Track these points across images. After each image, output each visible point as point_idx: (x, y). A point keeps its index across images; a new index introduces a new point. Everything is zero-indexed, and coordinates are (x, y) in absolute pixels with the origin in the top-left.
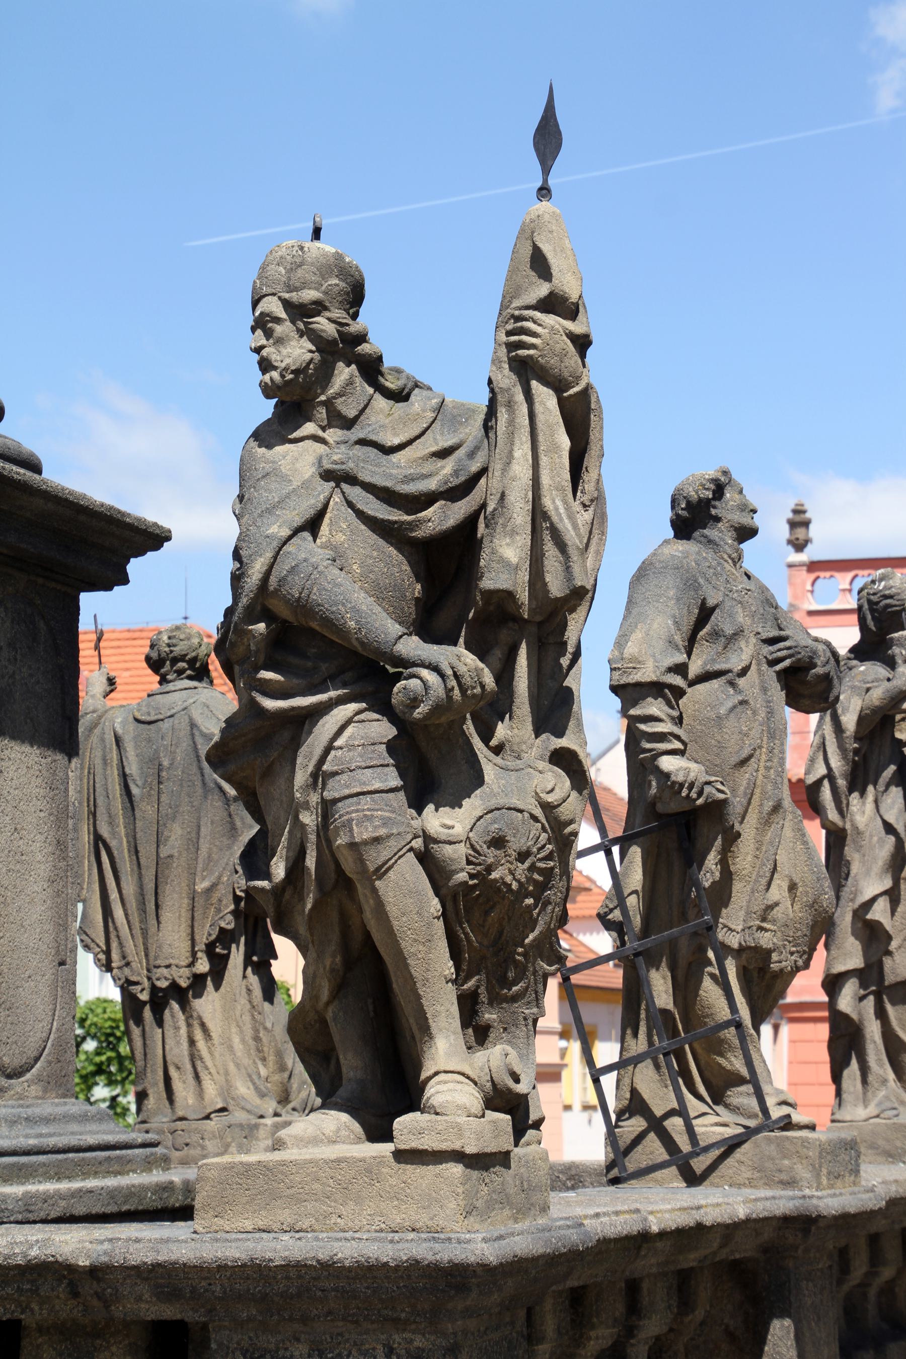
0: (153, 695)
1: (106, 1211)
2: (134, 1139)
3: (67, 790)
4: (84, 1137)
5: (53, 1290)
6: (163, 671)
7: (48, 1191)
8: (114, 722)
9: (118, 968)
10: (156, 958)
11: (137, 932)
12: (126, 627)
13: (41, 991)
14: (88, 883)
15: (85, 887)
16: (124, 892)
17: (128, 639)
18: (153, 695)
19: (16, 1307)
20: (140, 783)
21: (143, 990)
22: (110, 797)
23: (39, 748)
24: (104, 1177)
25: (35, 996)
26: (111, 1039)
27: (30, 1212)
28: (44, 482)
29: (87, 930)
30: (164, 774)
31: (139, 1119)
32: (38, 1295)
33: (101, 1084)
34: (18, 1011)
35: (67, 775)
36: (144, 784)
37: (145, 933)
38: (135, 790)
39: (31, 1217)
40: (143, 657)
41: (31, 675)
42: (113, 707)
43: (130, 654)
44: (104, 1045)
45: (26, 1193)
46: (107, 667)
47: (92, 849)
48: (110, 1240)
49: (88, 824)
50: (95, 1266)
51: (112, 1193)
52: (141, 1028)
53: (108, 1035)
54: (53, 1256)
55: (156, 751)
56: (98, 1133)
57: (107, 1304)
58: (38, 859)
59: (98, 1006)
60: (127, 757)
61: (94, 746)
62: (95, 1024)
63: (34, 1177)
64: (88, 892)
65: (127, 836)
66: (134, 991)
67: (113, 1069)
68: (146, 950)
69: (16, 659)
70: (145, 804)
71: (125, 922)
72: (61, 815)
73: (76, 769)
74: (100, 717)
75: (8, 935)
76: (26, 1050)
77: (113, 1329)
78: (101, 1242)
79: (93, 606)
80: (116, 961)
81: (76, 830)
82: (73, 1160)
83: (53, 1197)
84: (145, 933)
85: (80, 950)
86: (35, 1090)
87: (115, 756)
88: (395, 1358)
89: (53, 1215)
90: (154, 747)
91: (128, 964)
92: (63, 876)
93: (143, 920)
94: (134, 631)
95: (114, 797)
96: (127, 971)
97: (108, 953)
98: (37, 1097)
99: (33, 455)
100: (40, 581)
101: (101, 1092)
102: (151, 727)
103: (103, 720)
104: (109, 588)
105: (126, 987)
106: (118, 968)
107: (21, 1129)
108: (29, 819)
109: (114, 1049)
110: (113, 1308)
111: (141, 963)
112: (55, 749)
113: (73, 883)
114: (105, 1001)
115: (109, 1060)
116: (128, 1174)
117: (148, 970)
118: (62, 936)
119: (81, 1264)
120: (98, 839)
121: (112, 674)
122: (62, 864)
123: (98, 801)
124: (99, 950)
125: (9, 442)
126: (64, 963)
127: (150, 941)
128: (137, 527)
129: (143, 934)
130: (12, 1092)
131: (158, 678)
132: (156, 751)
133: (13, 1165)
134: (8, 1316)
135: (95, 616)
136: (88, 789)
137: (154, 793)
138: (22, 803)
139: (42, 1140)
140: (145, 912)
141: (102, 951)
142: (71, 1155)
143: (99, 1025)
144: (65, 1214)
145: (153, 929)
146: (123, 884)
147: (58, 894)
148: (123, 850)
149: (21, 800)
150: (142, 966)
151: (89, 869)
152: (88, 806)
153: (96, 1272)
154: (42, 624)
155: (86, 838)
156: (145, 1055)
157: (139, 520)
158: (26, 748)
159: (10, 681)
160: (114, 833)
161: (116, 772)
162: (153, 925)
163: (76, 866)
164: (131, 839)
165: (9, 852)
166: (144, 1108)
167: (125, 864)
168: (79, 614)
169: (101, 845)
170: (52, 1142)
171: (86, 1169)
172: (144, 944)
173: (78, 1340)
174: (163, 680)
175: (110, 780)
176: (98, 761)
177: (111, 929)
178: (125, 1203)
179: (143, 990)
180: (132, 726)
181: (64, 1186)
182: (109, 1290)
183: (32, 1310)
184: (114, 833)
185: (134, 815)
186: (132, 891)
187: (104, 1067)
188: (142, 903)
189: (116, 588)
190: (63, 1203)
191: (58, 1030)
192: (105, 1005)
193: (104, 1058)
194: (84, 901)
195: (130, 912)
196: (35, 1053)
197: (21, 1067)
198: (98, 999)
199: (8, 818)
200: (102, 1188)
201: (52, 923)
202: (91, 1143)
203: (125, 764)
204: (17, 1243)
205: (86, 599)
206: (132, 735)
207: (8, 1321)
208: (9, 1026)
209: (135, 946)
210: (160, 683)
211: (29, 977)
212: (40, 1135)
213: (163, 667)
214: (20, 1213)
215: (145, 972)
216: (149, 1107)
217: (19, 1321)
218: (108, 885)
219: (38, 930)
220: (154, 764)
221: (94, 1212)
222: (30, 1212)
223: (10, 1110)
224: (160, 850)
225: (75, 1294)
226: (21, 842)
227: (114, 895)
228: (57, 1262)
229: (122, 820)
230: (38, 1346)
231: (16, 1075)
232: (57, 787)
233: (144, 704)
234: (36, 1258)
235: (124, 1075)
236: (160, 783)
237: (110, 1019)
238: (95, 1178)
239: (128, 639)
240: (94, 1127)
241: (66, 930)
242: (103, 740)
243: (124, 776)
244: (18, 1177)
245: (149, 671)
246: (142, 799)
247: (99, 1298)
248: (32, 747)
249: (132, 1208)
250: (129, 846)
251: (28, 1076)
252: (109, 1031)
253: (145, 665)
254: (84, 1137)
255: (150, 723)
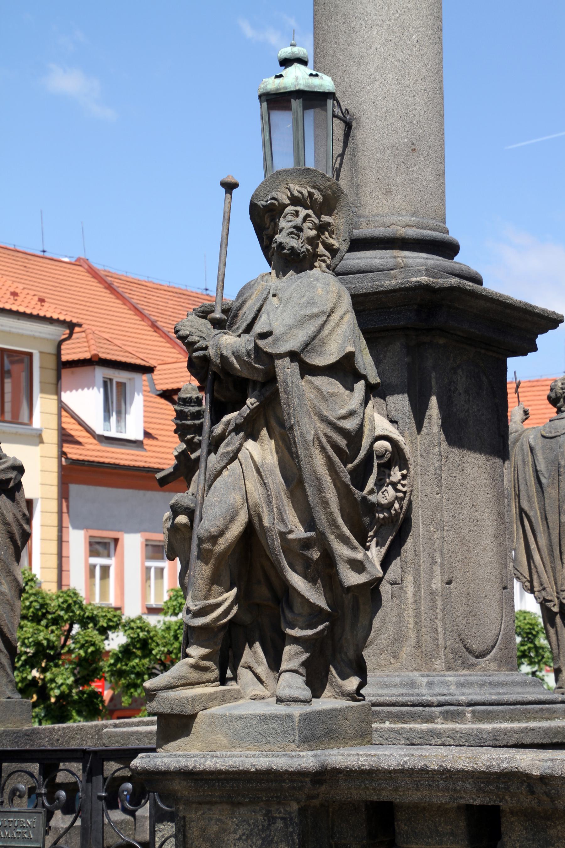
0: (553, 420)
1: (543, 742)
2: (556, 698)
3: (503, 480)
4: (525, 696)
5: (518, 789)
6: (559, 405)
7: (507, 728)
8: (529, 438)
9: (538, 591)
10: (562, 585)
11: (549, 569)
12: (528, 379)
13: (493, 604)
14: (517, 538)
15: (515, 541)
16: (539, 544)
17: (529, 387)
18: (553, 420)
19: (496, 798)
20: (546, 476)
21: (554, 605)
22: (528, 485)
23: (485, 455)
24: (540, 721)
25: (490, 607)
26: (530, 636)
27: (497, 740)
28: (485, 290)
29: (517, 568)
30: (562, 470)
31: (558, 686)
32: (509, 791)
33: (526, 663)
34: (480, 617)
35: (503, 471)
36: (549, 476)
37: (554, 569)
38: (544, 480)
39: (498, 743)
40: (546, 397)
41: (479, 410)
42: (528, 429)
43: (530, 396)
44: (526, 639)
45: (493, 729)
46: (524, 404)
47: (518, 517)
48: (551, 760)
49: (515, 502)
50: (543, 776)
51: (547, 731)
52: (555, 629)
53: (528, 634)
54: (516, 768)
55: (556, 456)
56: (534, 693)
57: (553, 801)
58: (487, 524)
59: (520, 616)
60: (538, 460)
61: (517, 453)
62: (519, 627)
63: (497, 719)
64: (517, 544)
65: (540, 509)
66: (549, 606)
67: (532, 654)
68: (555, 580)
69: (469, 401)
70: (550, 489)
71: (541, 562)
72: (500, 496)
73: (508, 467)
74: (520, 435)
75: (471, 570)
76: (486, 641)
77: (557, 815)
78: (546, 761)
79: (516, 366)
80: (537, 588)
81: (509, 505)
82: (520, 710)
83: (510, 732)
84: (554, 569)
85: (515, 580)
86: (493, 666)
87: (530, 459)
88: (254, 847)
89: (511, 743)
90: (555, 453)
91: (544, 589)
92: (502, 534)
93: (553, 561)
94: (533, 381)
95: (531, 484)
96: (544, 593)
97: (531, 582)
98: (494, 670)
99: (477, 274)
100: (483, 351)
101: (526, 668)
102: (553, 440)
103: (522, 437)
104: (525, 354)
105: (544, 604)
106: (538, 591)
107: (487, 689)
108: (481, 499)
109: (532, 642)
110: (556, 802)
111: (552, 588)
112: (495, 455)
113: (509, 538)
114: (525, 612)
115: (529, 649)
116: (555, 720)
117: (557, 593)
118: (504, 571)
119: (534, 773)
120: (522, 511)
121: (526, 408)
122: (502, 527)
123: (521, 488)
124: (526, 580)
125: (463, 267)
126: (506, 588)
127: (558, 574)
128: (542, 315)
129: (553, 570)
130: (480, 667)
131: (555, 410)
132: (556, 456)
133: (484, 711)
134: (492, 803)
135: (515, 372)
136: (514, 480)
137: (556, 482)
138: (476, 489)
139: (500, 696)
140: (553, 556)
141: (528, 581)
142: (518, 707)
143: (522, 627)
144: (518, 743)
145: (559, 567)
146: (539, 539)
147: (500, 545)
148: (538, 518)
149: (475, 487)
150: (553, 590)
151: (517, 530)
152: (515, 491)
153: (544, 779)
154: (484, 379)
155: (514, 511)
156: (558, 646)
157: (543, 310)
158: (478, 455)
159: (466, 414)
160: (531, 508)
161: (531, 469)
162: (559, 564)
163: (510, 527)
164: (542, 511)
165: (470, 519)
166: (560, 679)
167: (539, 525)
168: (507, 371)
169: (524, 515)
170: (506, 698)
171: (528, 715)
172: (554, 576)
173: (536, 820)
174: (559, 411)
175: (527, 474)
176: (520, 463)
177: (533, 567)
178: (554, 737)
179: (554, 605)
180: (540, 440)
181: (516, 725)
182: (553, 791)
183: (506, 800)
184: (531, 508)
185: (543, 496)
186: (544, 544)
187: (527, 653)
188: (551, 551)
189: (529, 354)
190: (516, 736)
191: (505, 629)
192: (525, 615)
193: (526, 648)
194: (515, 550)
195: (544, 556)
196: (492, 643)
197: (484, 651)
198: (520, 611)
199: (468, 499)
200: (540, 728)
201: (498, 563)
202: (530, 699)
203: (537, 464)
204: (494, 759)
205: (511, 361)
206: (540, 446)
207: (492, 806)
208: (475, 626)
209: (548, 577)
210: (557, 413)
211: (486, 596)
212: (499, 694)
213: (559, 403)
214: (491, 741)
215: (555, 594)
216: (563, 678)
217: (498, 807)
218: (529, 539)
219: (489, 567)
220: (555, 464)
221: (536, 742)
222: (497, 740)
223: (479, 678)
224: (561, 518)
225: (532, 792)
226: (476, 513)
227: (533, 546)
228: (519, 771)
229: (536, 499)
230: (512, 823)
231: (481, 656)
232: (497, 479)
233: (547, 426)
234: (506, 769)
235: (540, 658)
236: (559, 475)
237: (528, 623)
238: (534, 721)
239: (529, 387)
240: (531, 689)
241: (506, 567)
242: (522, 449)
243: (536, 472)
244: (487, 719)
245: (551, 406)
246: (548, 486)
247: (548, 796)
248: (481, 454)
249: (559, 741)
250: (541, 515)
251: (489, 657)
252: (528, 631)
253: (547, 402)
254: (525, 696)
255: (552, 438)
